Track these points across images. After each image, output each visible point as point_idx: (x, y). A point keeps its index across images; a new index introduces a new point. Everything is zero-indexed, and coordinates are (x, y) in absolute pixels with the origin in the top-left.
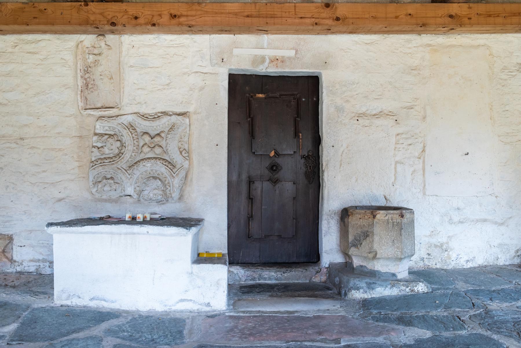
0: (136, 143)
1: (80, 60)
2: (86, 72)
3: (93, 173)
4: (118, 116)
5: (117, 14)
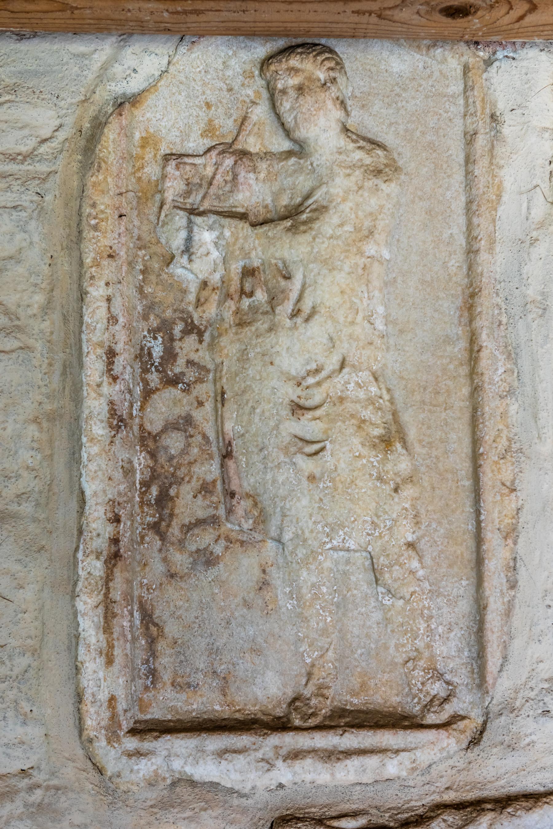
1: (108, 270)
2: (160, 370)
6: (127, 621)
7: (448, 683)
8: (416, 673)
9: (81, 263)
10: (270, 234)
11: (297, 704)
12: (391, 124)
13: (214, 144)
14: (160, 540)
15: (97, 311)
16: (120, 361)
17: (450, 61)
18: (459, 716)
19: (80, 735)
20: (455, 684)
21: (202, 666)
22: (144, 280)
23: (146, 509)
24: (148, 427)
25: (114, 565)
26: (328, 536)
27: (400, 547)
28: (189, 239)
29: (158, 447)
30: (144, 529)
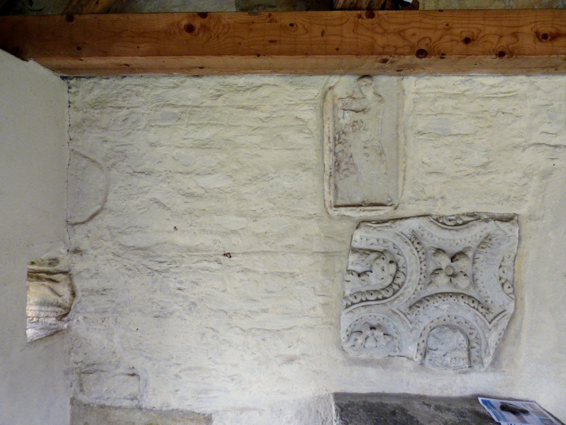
0: (424, 268)
2: (337, 141)
3: (347, 320)
4: (397, 219)
5: (430, 34)
6: (333, 187)
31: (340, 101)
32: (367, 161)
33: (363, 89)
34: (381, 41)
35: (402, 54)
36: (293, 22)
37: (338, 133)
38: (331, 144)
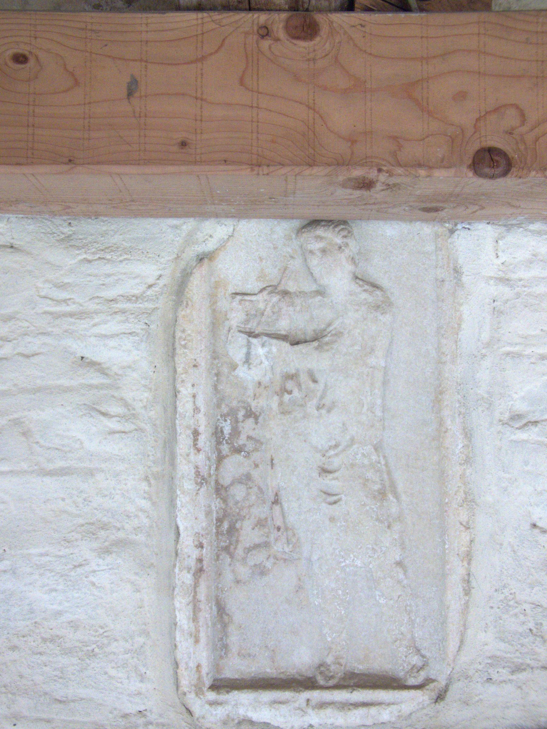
6: (207, 613)
7: (423, 656)
8: (401, 649)
9: (175, 371)
10: (304, 351)
11: (322, 669)
12: (386, 272)
13: (265, 286)
14: (230, 558)
15: (186, 405)
16: (202, 439)
17: (426, 230)
18: (431, 679)
19: (177, 689)
20: (428, 657)
21: (258, 642)
22: (217, 380)
23: (220, 537)
24: (221, 481)
25: (200, 577)
26: (343, 557)
27: (391, 566)
28: (248, 354)
29: (228, 495)
30: (219, 550)
31: (235, 304)
32: (332, 519)
33: (314, 262)
34: (341, 116)
35: (420, 165)
36: (23, 49)
37: (232, 413)
38: (201, 456)
